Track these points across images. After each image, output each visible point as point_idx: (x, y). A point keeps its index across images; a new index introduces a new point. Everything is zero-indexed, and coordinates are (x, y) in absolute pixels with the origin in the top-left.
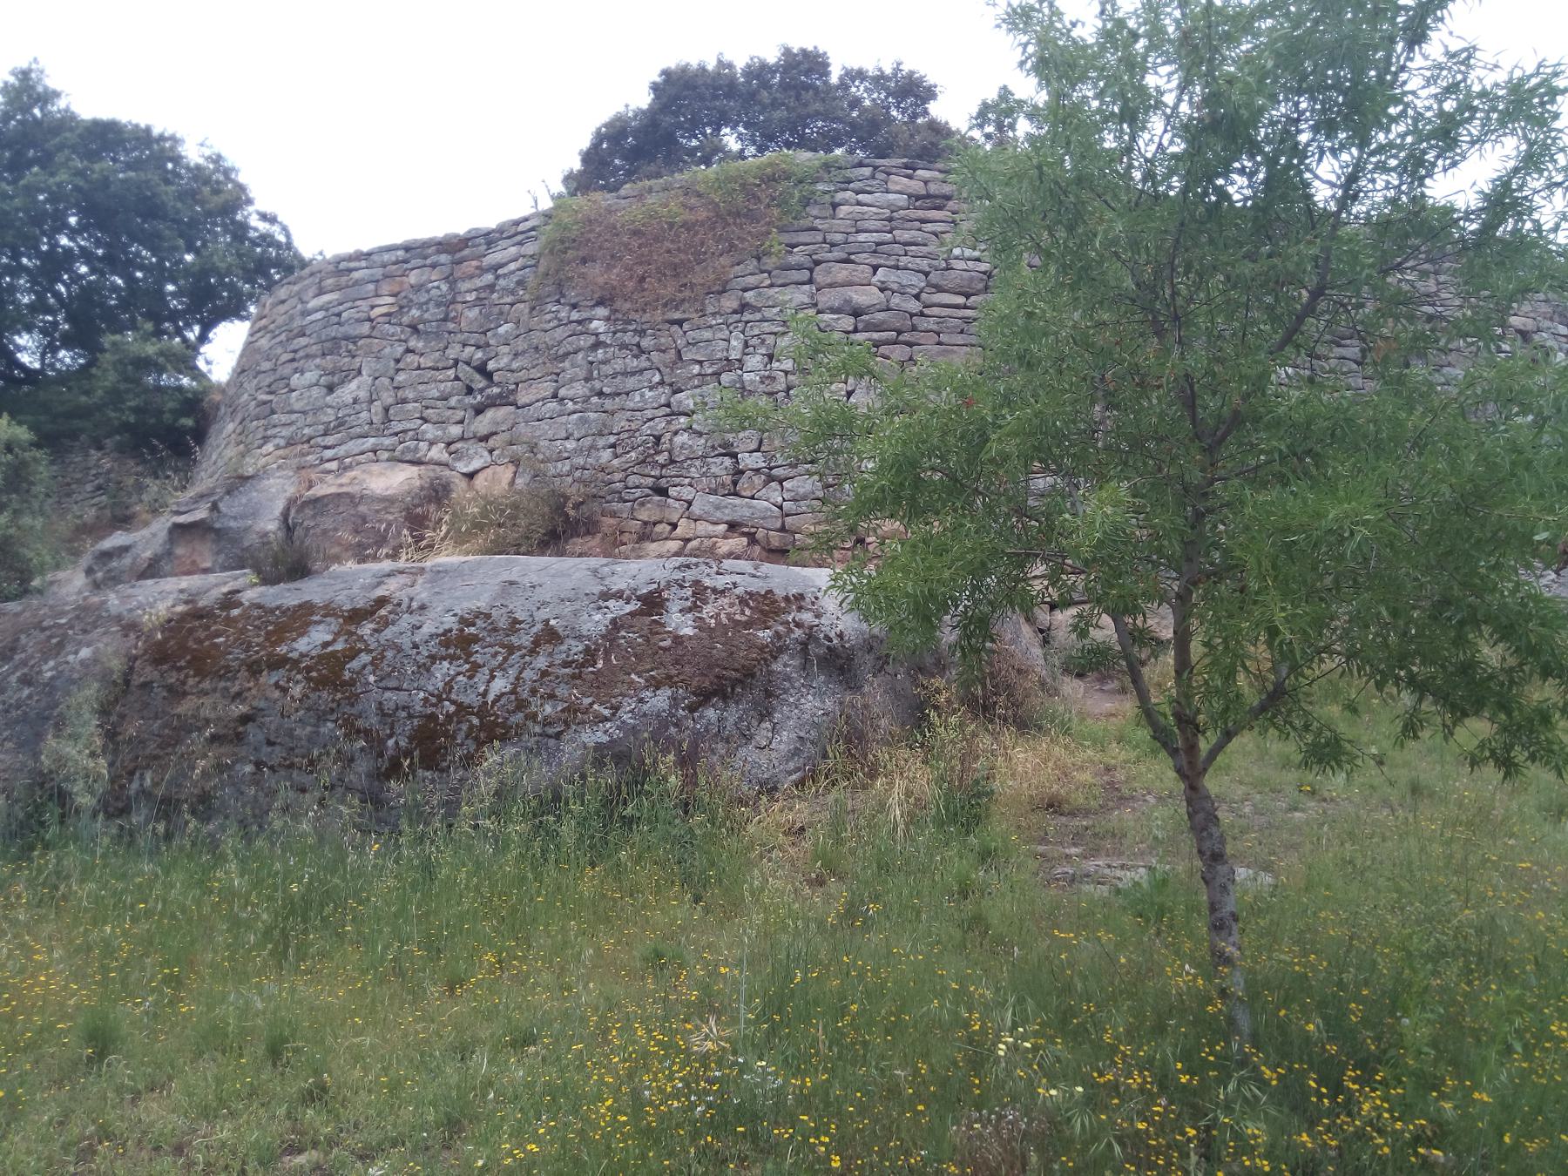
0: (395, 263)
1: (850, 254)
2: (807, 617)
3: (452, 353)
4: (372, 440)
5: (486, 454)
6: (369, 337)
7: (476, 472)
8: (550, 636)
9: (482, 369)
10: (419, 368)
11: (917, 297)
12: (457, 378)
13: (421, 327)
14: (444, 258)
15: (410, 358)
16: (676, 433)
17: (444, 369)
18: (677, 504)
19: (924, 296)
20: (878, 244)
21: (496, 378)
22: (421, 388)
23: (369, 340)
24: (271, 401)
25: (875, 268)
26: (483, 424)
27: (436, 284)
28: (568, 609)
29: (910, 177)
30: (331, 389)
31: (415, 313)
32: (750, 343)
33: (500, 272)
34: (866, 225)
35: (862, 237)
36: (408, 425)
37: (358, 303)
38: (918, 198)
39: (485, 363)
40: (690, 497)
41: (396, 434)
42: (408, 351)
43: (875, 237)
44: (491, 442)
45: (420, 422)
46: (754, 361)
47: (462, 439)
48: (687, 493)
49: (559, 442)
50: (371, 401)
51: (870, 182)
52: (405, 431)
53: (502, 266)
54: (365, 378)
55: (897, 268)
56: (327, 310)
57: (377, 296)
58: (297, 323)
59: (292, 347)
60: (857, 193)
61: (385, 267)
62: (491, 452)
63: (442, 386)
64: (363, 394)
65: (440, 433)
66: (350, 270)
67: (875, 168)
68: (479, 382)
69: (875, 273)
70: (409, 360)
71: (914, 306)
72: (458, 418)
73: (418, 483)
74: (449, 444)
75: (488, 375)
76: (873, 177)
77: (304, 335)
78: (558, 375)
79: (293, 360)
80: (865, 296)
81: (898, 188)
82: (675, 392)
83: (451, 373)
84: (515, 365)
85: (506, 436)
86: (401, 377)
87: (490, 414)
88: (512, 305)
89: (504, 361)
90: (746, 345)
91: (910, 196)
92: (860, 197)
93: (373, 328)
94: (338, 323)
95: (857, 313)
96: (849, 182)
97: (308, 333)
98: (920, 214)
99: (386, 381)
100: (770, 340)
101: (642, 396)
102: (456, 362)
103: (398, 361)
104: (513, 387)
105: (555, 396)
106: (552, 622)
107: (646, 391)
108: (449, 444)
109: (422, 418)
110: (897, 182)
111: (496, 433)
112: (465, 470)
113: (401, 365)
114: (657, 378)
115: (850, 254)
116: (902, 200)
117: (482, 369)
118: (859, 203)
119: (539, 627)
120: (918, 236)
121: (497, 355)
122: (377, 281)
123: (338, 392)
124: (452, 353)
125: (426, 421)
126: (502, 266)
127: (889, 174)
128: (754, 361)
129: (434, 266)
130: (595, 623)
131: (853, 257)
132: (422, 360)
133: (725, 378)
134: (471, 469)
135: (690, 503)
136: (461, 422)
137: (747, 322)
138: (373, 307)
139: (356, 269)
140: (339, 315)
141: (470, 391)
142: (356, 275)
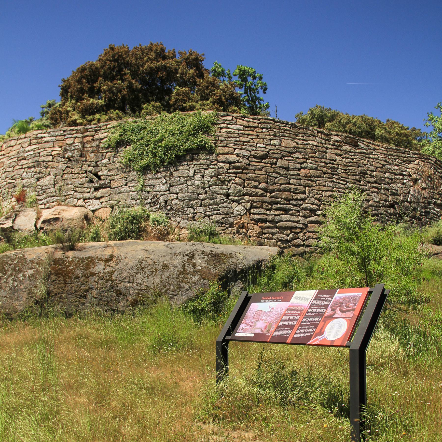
0: (60, 136)
1: (227, 144)
2: (234, 260)
3: (85, 168)
4: (56, 198)
5: (100, 204)
6: (52, 161)
7: (97, 210)
8: (166, 267)
9: (96, 175)
10: (72, 173)
11: (248, 159)
12: (87, 177)
13: (72, 159)
14: (79, 135)
15: (69, 169)
16: (173, 200)
17: (81, 174)
18: (174, 223)
19: (250, 159)
20: (235, 141)
21: (102, 178)
22: (73, 180)
23: (53, 163)
24: (14, 183)
25: (235, 149)
26: (98, 194)
27: (77, 144)
28: (168, 258)
29: (243, 120)
30: (38, 180)
31: (70, 154)
32: (196, 171)
33: (102, 141)
34: (232, 135)
35: (230, 139)
36: (69, 193)
37: (46, 149)
38: (246, 127)
39: (97, 173)
40: (179, 221)
41: (65, 196)
42: (67, 167)
43: (234, 139)
44: (102, 200)
45: (74, 192)
46: (198, 177)
47: (89, 198)
48: (178, 220)
49: (129, 201)
50: (55, 184)
51: (232, 121)
52: (68, 195)
53: (102, 139)
54: (52, 176)
55: (241, 149)
56: (34, 151)
57: (53, 147)
58: (22, 154)
59: (21, 164)
60: (228, 124)
61: (56, 137)
62: (101, 203)
63: (81, 180)
64: (52, 182)
65: (81, 196)
66: (42, 137)
67: (233, 116)
68: (95, 179)
69: (235, 151)
70: (68, 170)
71: (247, 162)
72: (88, 191)
73: (79, 214)
74: (84, 200)
75: (99, 177)
76: (232, 120)
77: (25, 159)
78: (127, 178)
79: (22, 168)
80: (233, 158)
81: (240, 124)
82: (170, 186)
83: (84, 175)
84: (109, 174)
85: (108, 198)
86: (66, 176)
87: (101, 191)
88: (107, 153)
89: (105, 172)
90: (195, 172)
91: (244, 126)
92: (229, 126)
93: (53, 158)
94: (39, 156)
95: (230, 163)
96: (225, 121)
97: (27, 159)
98: (247, 132)
99: (60, 177)
100: (203, 171)
101: (160, 187)
102: (86, 172)
103: (64, 171)
104: (109, 181)
105: (126, 185)
106: (165, 262)
107: (161, 185)
108: (84, 200)
109: (74, 191)
110: (240, 122)
111: (104, 197)
112: (92, 209)
113: (65, 172)
114: (164, 181)
115: (227, 144)
116: (241, 128)
117: (96, 175)
118: (228, 128)
119: (162, 264)
120: (247, 139)
121: (102, 170)
122: (54, 142)
123: (42, 180)
124: (85, 168)
125: (76, 191)
126: (102, 139)
127: (237, 119)
128: (198, 177)
129: (75, 138)
130: (178, 261)
131: (228, 145)
132: (73, 170)
133: (189, 183)
134: (95, 209)
135: (179, 223)
136: (89, 192)
137: (195, 165)
138: (52, 151)
139: (45, 137)
140: (39, 153)
141: (91, 181)
142: (45, 139)
